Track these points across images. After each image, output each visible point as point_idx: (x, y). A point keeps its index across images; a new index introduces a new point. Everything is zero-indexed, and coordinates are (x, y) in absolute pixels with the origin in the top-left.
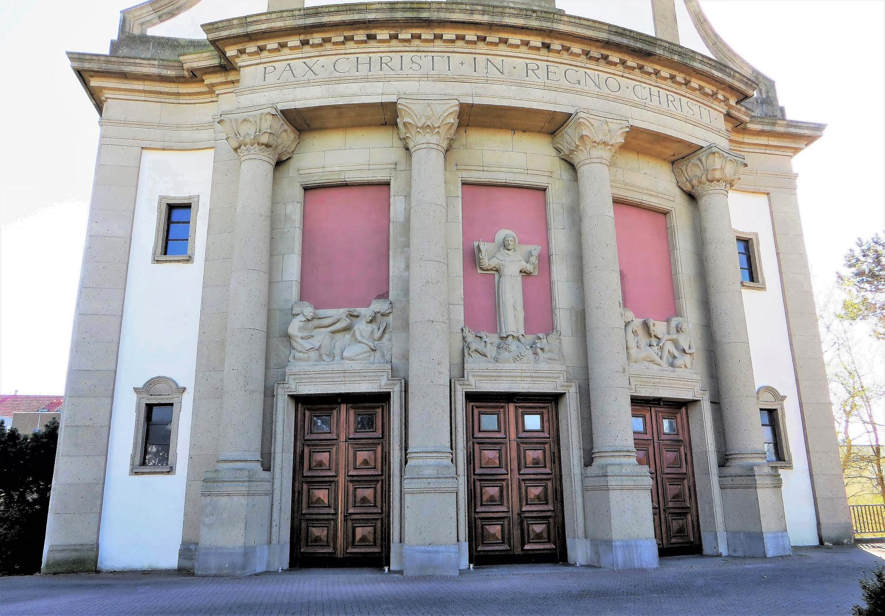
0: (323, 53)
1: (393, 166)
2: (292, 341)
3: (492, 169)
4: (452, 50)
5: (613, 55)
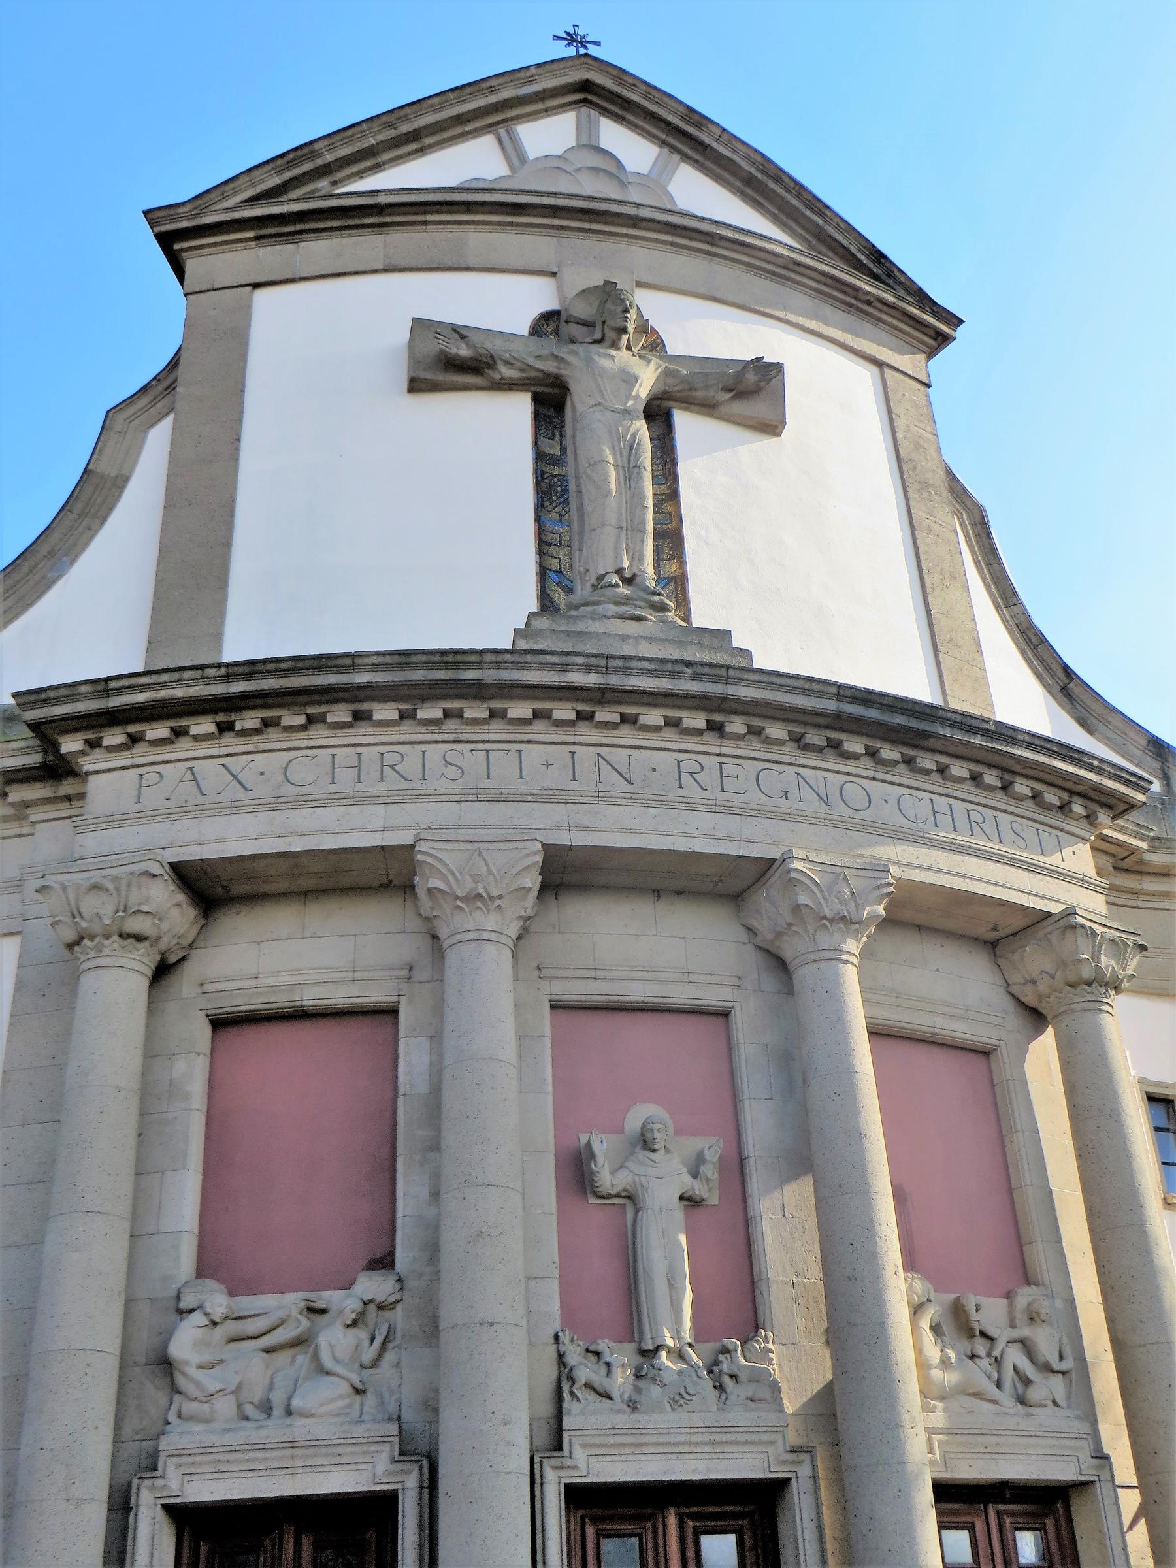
0: (263, 747)
1: (405, 973)
2: (177, 1375)
3: (615, 974)
4: (525, 737)
5: (852, 739)
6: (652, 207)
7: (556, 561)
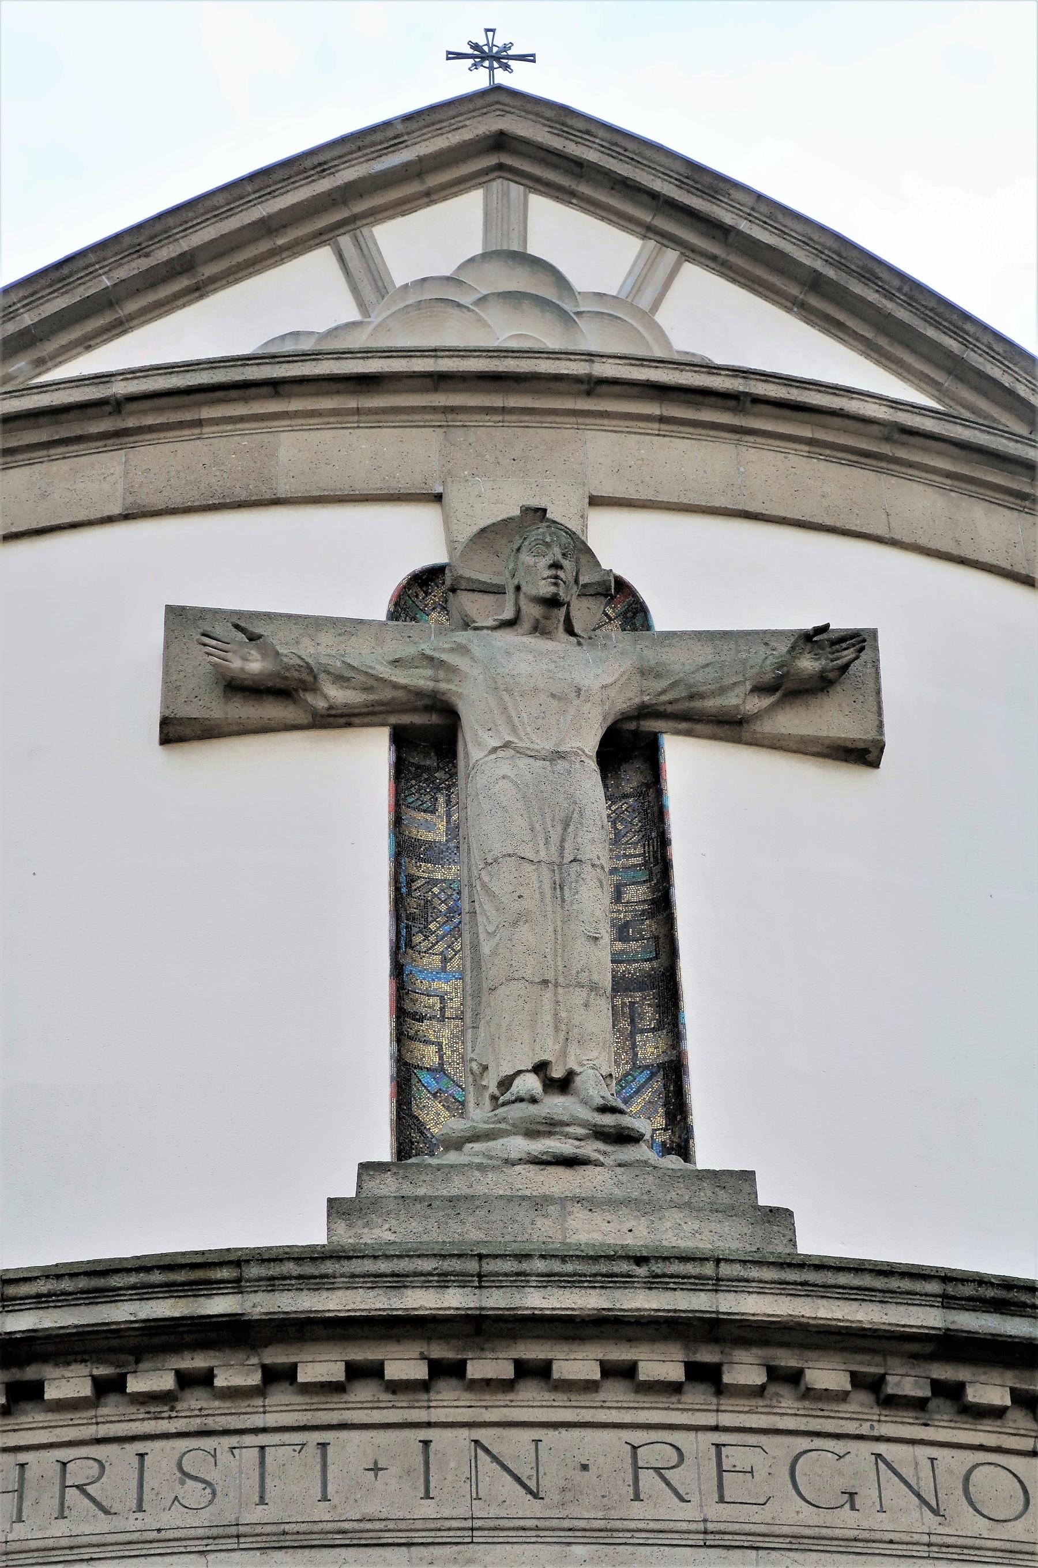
4: (334, 1418)
5: (983, 1378)
6: (620, 358)
7: (433, 1048)
